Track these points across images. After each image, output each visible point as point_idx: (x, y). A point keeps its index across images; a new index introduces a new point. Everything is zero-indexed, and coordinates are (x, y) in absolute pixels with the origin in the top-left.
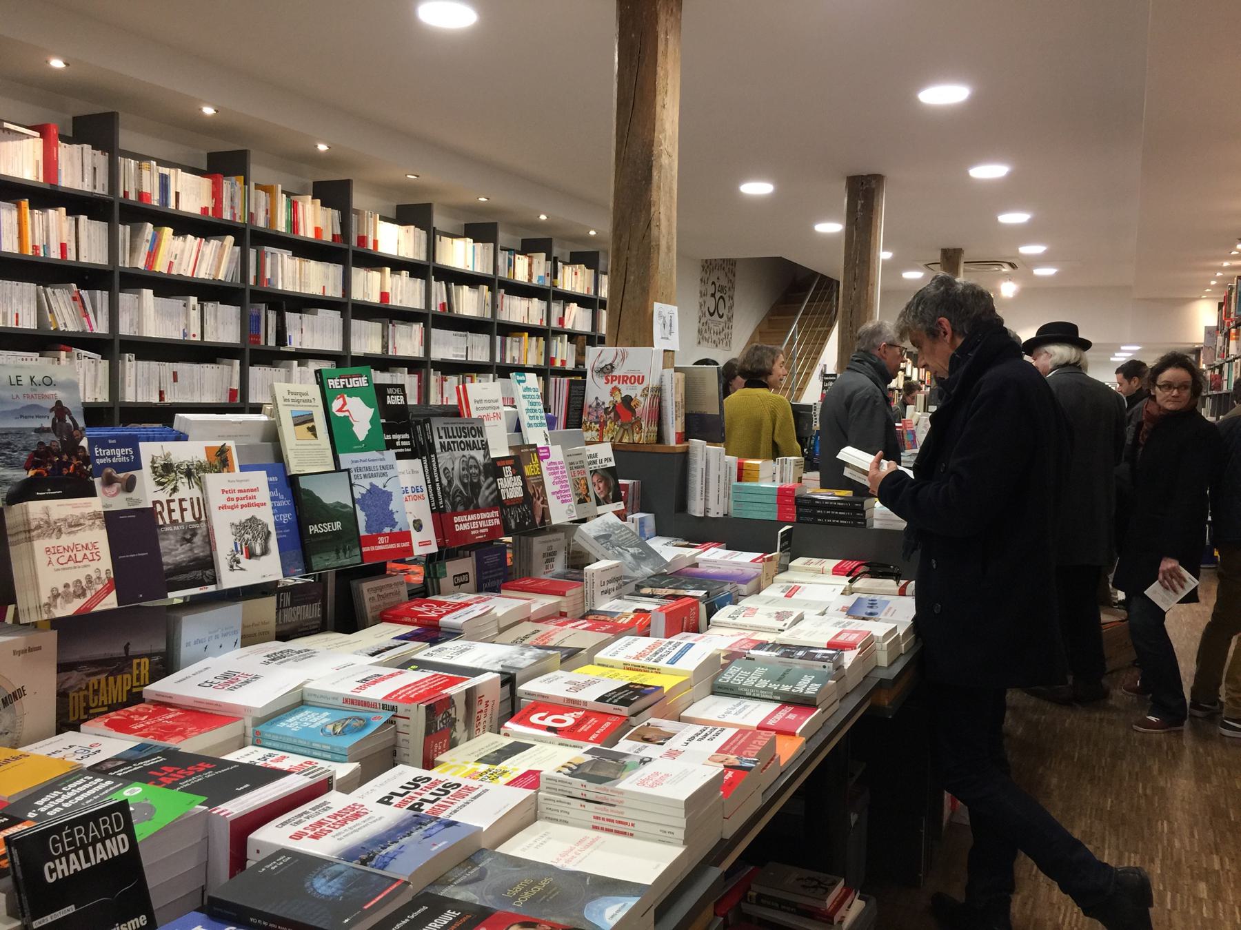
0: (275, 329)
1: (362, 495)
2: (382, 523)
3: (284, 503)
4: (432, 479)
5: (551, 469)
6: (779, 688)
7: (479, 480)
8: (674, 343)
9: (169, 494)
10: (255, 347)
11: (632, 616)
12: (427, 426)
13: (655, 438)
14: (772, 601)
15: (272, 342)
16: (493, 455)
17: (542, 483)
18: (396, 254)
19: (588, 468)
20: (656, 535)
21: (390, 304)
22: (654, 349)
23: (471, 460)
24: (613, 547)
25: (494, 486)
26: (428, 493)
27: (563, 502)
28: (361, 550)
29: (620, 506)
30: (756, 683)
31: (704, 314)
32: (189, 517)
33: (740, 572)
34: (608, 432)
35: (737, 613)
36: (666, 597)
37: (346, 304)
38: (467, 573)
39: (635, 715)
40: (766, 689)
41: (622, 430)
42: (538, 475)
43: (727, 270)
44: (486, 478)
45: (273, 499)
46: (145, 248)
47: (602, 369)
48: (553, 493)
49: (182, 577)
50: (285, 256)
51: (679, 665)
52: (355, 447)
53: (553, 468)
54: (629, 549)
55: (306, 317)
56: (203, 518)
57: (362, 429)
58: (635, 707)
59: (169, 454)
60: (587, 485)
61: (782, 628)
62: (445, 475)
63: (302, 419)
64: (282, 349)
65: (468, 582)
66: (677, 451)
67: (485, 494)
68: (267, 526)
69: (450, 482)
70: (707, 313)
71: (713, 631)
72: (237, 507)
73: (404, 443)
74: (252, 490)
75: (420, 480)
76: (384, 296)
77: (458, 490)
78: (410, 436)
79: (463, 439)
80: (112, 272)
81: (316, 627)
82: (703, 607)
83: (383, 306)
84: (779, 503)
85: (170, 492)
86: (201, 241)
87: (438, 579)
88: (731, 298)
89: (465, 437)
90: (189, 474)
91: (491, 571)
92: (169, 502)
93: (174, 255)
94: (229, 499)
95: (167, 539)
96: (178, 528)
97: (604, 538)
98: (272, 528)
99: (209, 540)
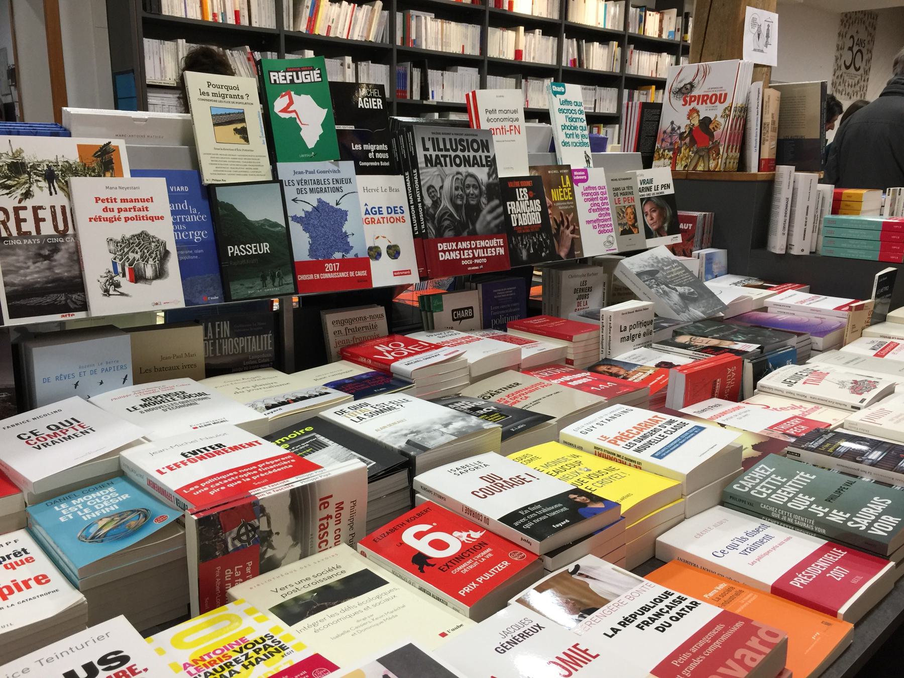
0: (419, 85)
1: (306, 212)
2: (331, 247)
3: (196, 218)
4: (415, 199)
5: (588, 194)
6: (826, 514)
7: (479, 202)
8: (770, 57)
9: (17, 199)
10: (402, 101)
11: (651, 372)
12: (410, 135)
13: (736, 166)
14: (856, 360)
15: (416, 96)
16: (501, 175)
17: (575, 210)
18: (530, 14)
19: (638, 196)
20: (728, 274)
21: (523, 60)
22: (741, 61)
23: (469, 179)
24: (658, 285)
25: (500, 210)
26: (411, 215)
27: (601, 232)
28: (295, 278)
29: (678, 239)
30: (790, 500)
31: (839, 68)
32: (47, 229)
33: (819, 321)
34: (682, 159)
35: (797, 377)
36: (705, 350)
37: (483, 61)
38: (472, 308)
39: (552, 554)
40: (805, 513)
41: (697, 156)
42: (568, 200)
43: (867, 23)
44: (490, 200)
45: (173, 213)
46: (306, 13)
47: (680, 90)
48: (588, 222)
49: (34, 301)
50: (428, 18)
51: (668, 462)
52: (303, 156)
53: (590, 194)
54: (678, 288)
55: (447, 74)
56: (71, 231)
57: (311, 134)
58: (553, 541)
59: (20, 151)
60: (635, 214)
61: (857, 404)
62: (429, 194)
63: (227, 119)
64: (425, 102)
65: (472, 317)
66: (759, 179)
67: (487, 217)
68: (164, 244)
69: (436, 203)
70: (843, 67)
71: (759, 399)
72: (119, 219)
73: (378, 155)
74: (143, 200)
75: (401, 199)
76: (518, 53)
77: (446, 211)
78: (390, 147)
79: (459, 153)
80: (279, 35)
81: (268, 360)
82: (749, 367)
83: (517, 63)
84: (882, 239)
85: (19, 197)
86: (354, 6)
87: (432, 312)
88: (870, 51)
89: (463, 151)
90: (50, 176)
91: (503, 307)
92: (16, 210)
93: (331, 20)
94: (105, 210)
95: (14, 255)
96: (30, 242)
97: (649, 275)
98: (172, 247)
99: (76, 257)
